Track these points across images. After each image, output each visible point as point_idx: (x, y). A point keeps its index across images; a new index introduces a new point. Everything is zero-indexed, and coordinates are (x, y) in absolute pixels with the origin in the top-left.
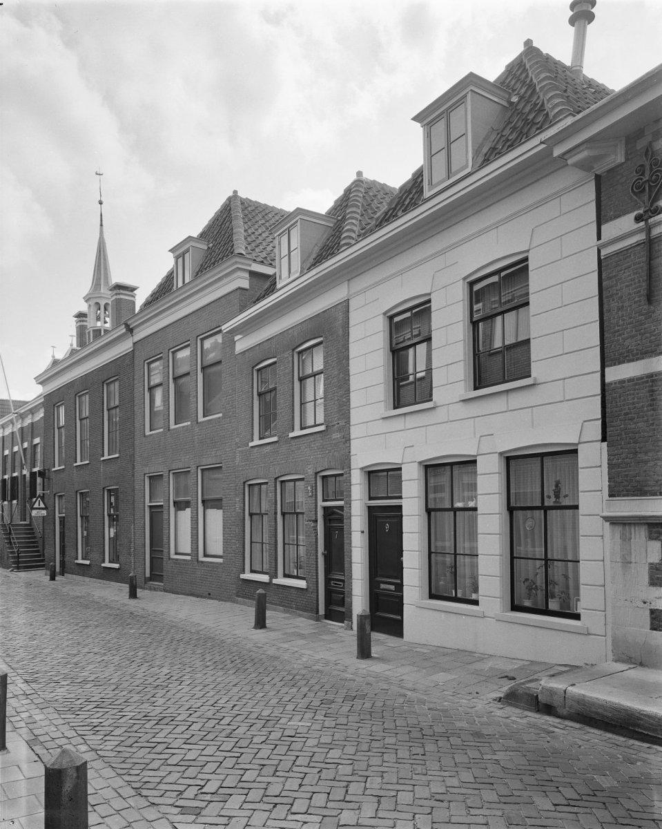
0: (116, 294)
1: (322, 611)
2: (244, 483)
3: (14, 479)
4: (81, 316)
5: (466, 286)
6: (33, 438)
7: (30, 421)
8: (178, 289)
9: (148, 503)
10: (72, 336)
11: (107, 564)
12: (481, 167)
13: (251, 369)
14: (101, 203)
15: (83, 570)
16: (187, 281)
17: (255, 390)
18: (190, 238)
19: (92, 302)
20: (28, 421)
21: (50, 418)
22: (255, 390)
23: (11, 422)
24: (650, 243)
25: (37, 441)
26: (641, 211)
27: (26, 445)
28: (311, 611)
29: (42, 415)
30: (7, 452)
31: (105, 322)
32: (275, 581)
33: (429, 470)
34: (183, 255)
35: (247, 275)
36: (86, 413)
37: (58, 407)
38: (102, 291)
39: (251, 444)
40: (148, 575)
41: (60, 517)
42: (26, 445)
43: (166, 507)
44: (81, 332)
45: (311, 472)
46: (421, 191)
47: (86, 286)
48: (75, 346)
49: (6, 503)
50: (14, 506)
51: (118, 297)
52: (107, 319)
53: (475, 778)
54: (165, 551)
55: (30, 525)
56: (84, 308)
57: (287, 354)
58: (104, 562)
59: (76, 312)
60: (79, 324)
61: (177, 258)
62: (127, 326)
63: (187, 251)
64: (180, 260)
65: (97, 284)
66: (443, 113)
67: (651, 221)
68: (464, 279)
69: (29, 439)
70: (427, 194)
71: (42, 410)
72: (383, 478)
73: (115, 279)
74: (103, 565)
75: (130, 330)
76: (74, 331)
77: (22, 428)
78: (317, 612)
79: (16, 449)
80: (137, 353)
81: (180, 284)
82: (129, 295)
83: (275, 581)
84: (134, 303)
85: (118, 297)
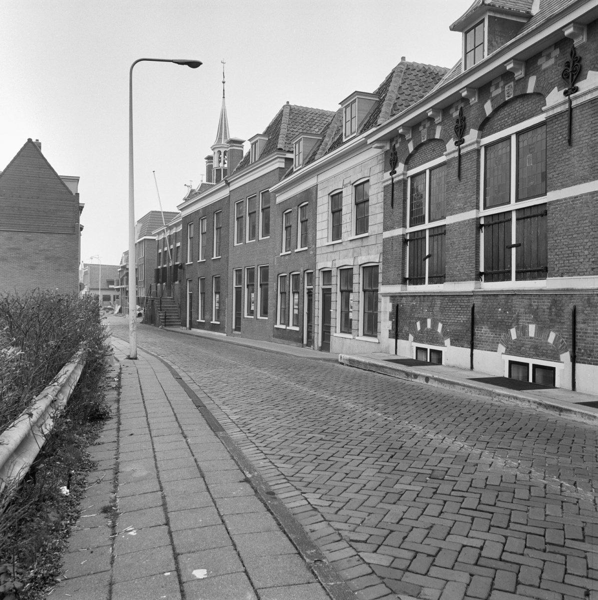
0: (231, 146)
1: (305, 342)
2: (290, 273)
3: (164, 269)
4: (210, 158)
5: (354, 188)
6: (176, 242)
7: (174, 232)
8: (252, 164)
9: (234, 286)
10: (202, 175)
11: (214, 322)
12: (362, 132)
13: (281, 213)
14: (224, 83)
15: (200, 326)
16: (256, 160)
17: (284, 225)
18: (258, 135)
19: (216, 151)
20: (174, 231)
21: (185, 230)
22: (284, 225)
23: (163, 231)
24: (571, 109)
25: (178, 244)
26: (567, 89)
27: (172, 247)
28: (300, 342)
29: (181, 228)
30: (160, 251)
31: (224, 163)
32: (288, 328)
33: (342, 271)
34: (255, 143)
35: (284, 160)
36: (205, 230)
37: (190, 225)
38: (223, 143)
39: (281, 254)
40: (234, 327)
41: (190, 294)
42: (172, 247)
43: (243, 288)
44: (209, 168)
45: (302, 270)
46: (342, 139)
47: (213, 140)
48: (205, 182)
49: (159, 284)
50: (164, 287)
51: (232, 148)
52: (226, 161)
53: (588, 568)
54: (242, 313)
55: (173, 299)
56: (211, 153)
57: (296, 208)
58: (212, 320)
59: (206, 156)
60: (208, 164)
61: (252, 144)
62: (226, 181)
63: (257, 141)
64: (254, 146)
65: (219, 139)
66: (349, 104)
67: (461, 146)
68: (329, 194)
69: (174, 243)
70: (344, 140)
71: (181, 226)
72: (327, 274)
73: (233, 135)
74: (211, 322)
75: (228, 184)
76: (204, 171)
77: (170, 236)
78: (303, 342)
79: (166, 249)
80: (231, 197)
81: (253, 161)
82: (238, 147)
83: (288, 328)
84: (242, 151)
85: (232, 148)
